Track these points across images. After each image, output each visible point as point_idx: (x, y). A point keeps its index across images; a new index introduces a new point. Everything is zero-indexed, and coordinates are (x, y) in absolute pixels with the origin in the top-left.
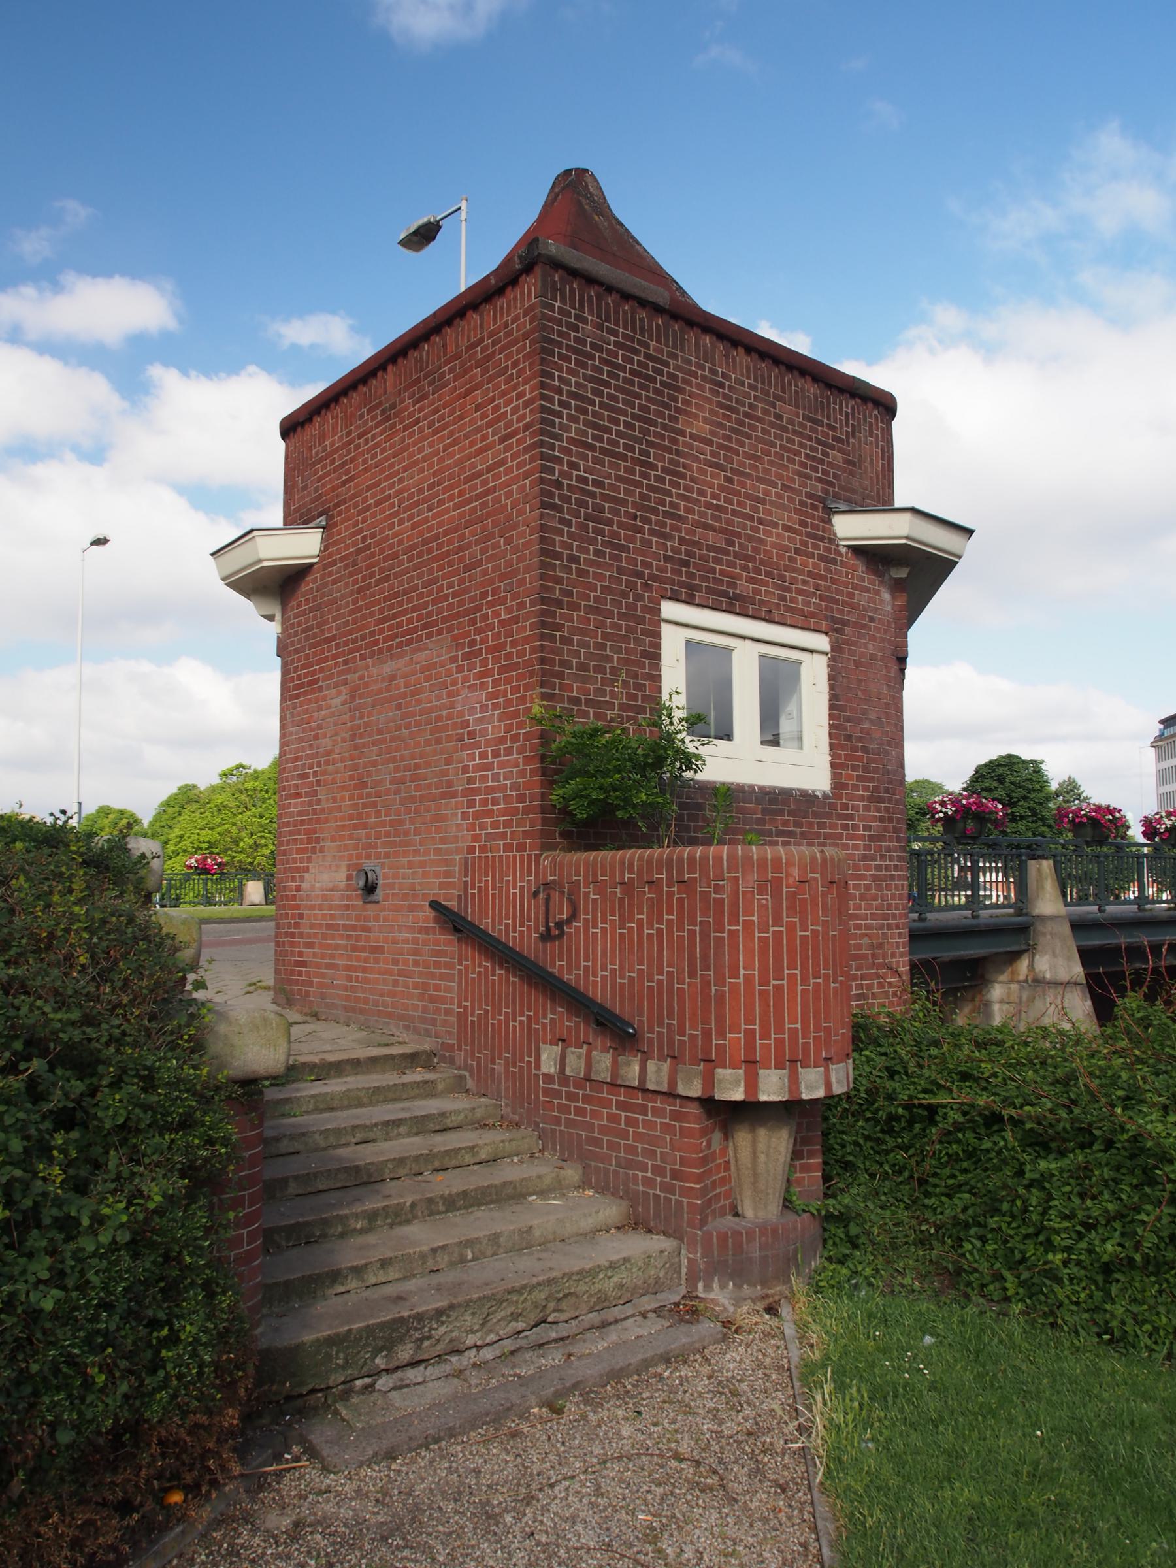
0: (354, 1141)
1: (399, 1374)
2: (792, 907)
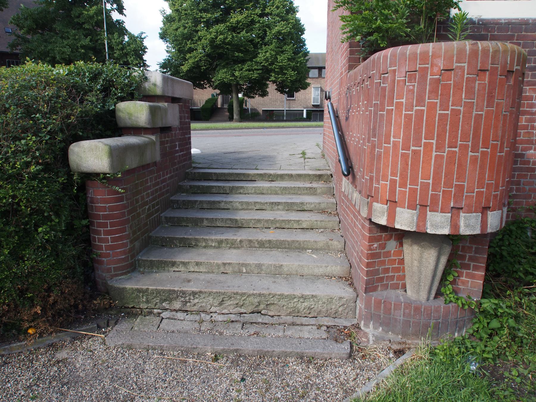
1: (174, 313)
2: (434, 92)
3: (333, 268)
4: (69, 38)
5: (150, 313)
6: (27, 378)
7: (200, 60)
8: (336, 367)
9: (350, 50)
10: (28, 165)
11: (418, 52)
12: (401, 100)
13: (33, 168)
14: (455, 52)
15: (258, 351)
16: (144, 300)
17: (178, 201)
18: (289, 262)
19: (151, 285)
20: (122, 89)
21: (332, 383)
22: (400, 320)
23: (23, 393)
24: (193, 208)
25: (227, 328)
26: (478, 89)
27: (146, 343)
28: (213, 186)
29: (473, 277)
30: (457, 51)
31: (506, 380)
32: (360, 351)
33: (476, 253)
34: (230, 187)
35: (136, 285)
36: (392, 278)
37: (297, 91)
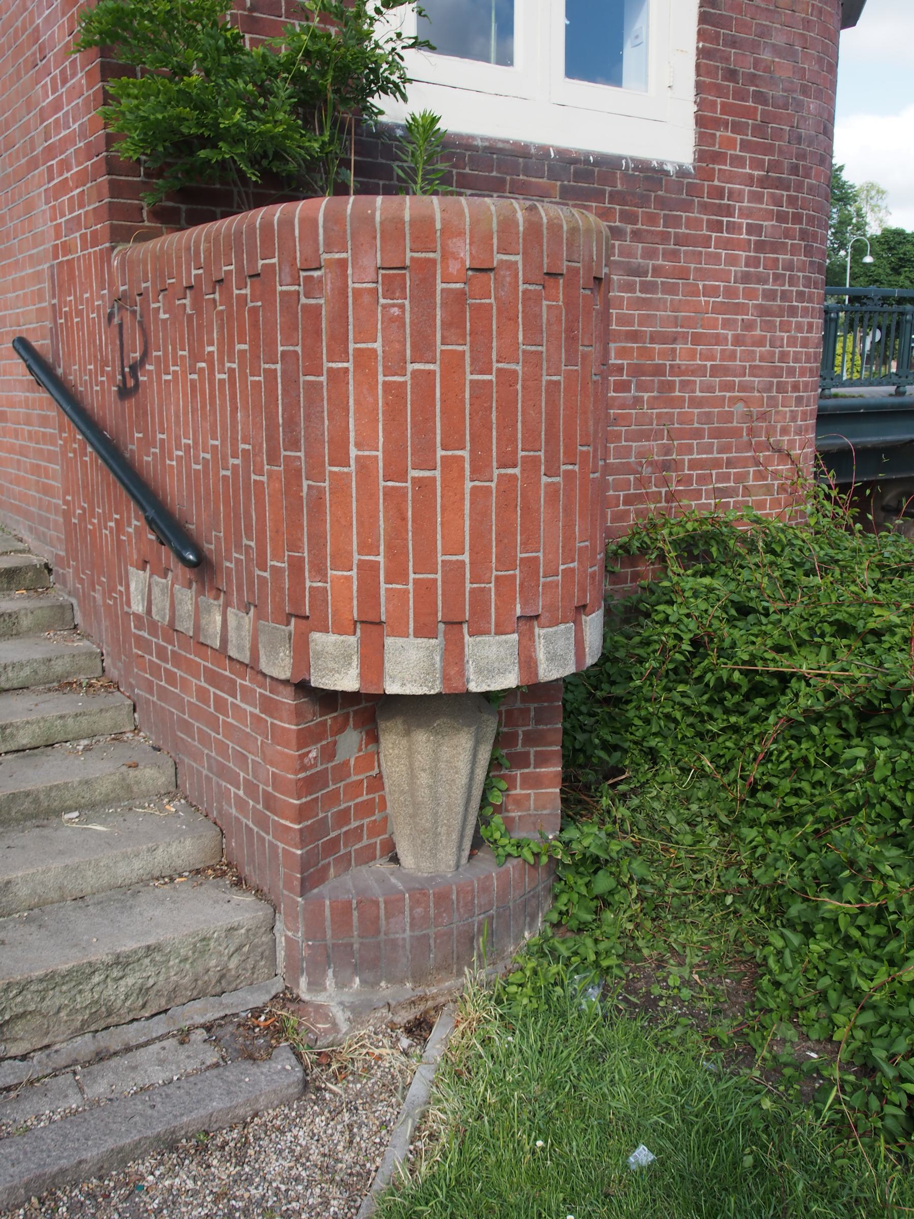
2: (454, 324)
3: (173, 850)
11: (407, 218)
12: (370, 345)
15: (27, 1186)
21: (298, 1179)
22: (404, 939)
26: (548, 319)
29: (534, 782)
30: (498, 223)
31: (662, 1004)
32: (324, 1061)
33: (538, 722)
36: (357, 834)
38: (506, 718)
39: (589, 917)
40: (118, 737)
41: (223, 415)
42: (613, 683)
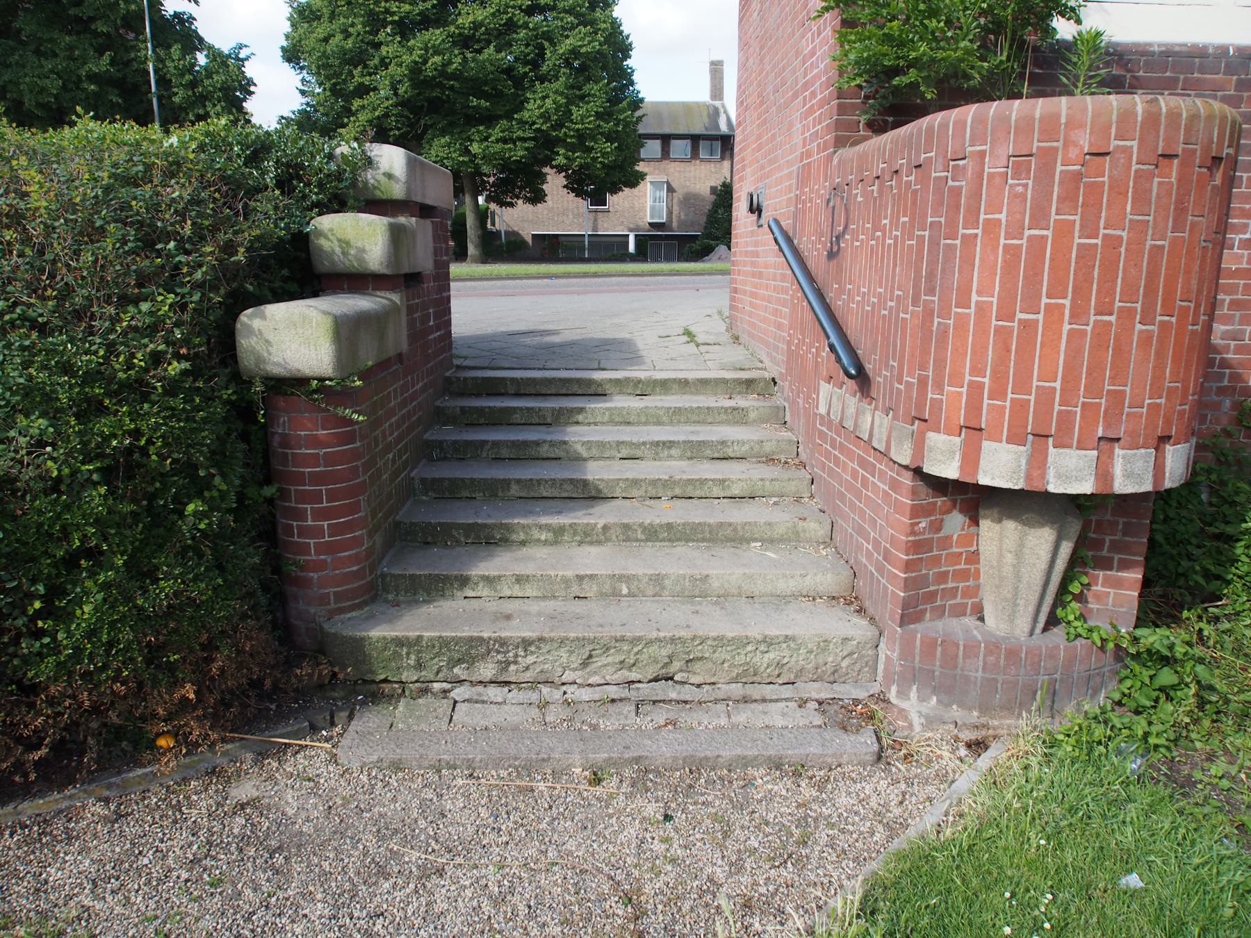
0: (620, 456)
1: (480, 688)
2: (1068, 198)
4: (55, 55)
5: (425, 691)
6: (179, 844)
7: (386, 115)
8: (855, 782)
9: (839, 105)
10: (156, 359)
11: (1037, 115)
12: (996, 216)
13: (175, 368)
14: (1114, 118)
15: (684, 759)
16: (412, 662)
17: (441, 442)
18: (723, 568)
19: (426, 630)
20: (320, 185)
23: (185, 875)
24: (476, 457)
25: (603, 716)
27: (432, 756)
28: (515, 408)
29: (1118, 584)
31: (1199, 786)
32: (898, 747)
33: (1125, 534)
34: (553, 409)
35: (393, 630)
36: (953, 592)
37: (615, 190)
38: (1091, 524)
39: (1148, 703)
40: (798, 499)
41: (888, 271)
42: (1227, 523)
